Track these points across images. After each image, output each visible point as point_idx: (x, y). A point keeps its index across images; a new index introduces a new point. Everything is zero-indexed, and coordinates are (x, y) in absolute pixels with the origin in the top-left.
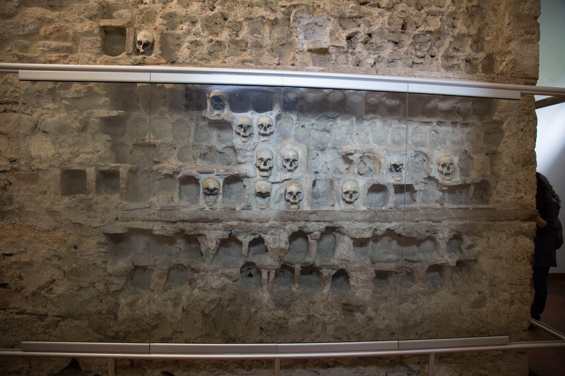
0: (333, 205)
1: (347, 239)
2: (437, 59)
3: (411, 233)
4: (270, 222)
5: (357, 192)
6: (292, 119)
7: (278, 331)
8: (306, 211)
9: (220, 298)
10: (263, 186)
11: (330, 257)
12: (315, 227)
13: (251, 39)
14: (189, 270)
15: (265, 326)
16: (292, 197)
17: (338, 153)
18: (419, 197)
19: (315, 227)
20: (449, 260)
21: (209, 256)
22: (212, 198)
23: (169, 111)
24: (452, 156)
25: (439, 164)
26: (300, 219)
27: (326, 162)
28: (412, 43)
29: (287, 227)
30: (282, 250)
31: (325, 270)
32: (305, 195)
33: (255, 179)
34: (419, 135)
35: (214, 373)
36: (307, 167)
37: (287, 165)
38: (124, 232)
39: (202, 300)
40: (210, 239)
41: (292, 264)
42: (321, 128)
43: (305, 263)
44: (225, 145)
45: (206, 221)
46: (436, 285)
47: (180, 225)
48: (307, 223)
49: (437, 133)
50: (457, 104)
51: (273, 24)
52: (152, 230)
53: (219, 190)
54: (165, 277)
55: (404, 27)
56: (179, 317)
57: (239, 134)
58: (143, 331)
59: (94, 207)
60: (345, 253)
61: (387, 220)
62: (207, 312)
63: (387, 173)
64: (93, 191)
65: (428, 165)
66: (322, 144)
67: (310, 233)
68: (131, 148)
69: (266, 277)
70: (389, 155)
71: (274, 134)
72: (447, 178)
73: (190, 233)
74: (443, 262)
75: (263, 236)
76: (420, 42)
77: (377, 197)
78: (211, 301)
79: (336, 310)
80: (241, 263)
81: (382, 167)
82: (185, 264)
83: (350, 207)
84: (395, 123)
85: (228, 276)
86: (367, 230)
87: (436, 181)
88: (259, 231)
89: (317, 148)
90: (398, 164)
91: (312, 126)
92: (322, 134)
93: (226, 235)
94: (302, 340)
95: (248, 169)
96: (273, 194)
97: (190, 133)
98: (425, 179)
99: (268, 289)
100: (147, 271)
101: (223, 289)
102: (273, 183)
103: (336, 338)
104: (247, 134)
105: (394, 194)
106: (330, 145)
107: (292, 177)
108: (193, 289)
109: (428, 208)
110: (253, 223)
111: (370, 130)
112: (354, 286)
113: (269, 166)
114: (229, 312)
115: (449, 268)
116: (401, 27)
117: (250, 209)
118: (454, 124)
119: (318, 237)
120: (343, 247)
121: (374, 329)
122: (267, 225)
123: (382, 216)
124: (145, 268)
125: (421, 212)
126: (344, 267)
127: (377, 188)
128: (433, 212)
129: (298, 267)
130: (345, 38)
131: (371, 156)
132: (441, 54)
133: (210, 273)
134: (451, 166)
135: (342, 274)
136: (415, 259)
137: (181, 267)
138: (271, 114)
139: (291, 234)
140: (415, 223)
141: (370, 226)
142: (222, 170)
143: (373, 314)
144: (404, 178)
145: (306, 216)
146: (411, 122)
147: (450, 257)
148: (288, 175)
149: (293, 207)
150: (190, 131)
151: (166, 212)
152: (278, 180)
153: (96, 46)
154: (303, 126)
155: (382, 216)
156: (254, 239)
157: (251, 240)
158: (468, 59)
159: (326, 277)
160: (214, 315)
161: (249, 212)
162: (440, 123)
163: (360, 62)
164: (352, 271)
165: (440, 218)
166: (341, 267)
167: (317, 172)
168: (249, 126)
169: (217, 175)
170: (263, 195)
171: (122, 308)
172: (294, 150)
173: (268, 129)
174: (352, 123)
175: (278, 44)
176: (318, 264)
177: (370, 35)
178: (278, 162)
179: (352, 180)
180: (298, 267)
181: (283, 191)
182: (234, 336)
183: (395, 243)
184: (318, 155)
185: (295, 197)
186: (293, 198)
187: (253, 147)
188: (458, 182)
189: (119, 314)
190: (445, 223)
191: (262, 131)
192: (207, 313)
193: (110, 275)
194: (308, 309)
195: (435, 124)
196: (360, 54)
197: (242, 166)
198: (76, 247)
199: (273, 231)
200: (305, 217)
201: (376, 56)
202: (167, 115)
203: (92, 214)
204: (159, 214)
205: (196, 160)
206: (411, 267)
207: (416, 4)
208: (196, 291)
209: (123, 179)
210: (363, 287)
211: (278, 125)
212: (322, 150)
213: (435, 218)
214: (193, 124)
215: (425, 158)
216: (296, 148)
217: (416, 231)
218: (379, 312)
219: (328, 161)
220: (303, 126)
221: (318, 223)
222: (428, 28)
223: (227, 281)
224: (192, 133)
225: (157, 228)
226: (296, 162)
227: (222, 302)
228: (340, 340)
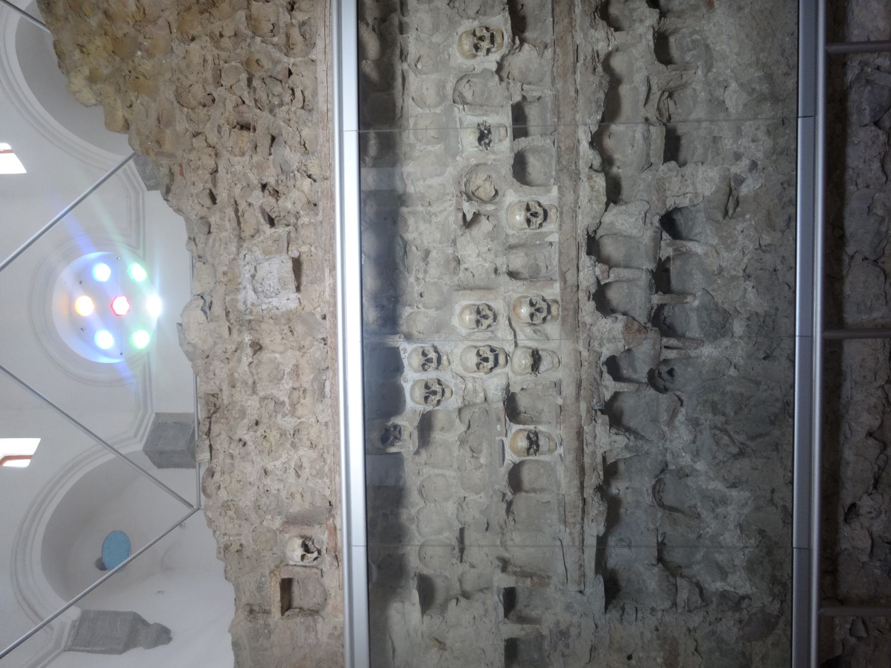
0: (551, 244)
1: (608, 218)
2: (293, 64)
3: (597, 102)
4: (581, 349)
5: (528, 205)
6: (411, 313)
7: (770, 332)
8: (561, 290)
9: (711, 429)
10: (522, 360)
11: (640, 242)
12: (589, 273)
13: (287, 384)
14: (662, 476)
15: (761, 352)
16: (538, 314)
17: (462, 235)
18: (533, 92)
19: (589, 273)
20: (648, 23)
21: (639, 445)
22: (542, 442)
23: (407, 508)
24: (461, 30)
25: (475, 56)
26: (575, 300)
27: (478, 255)
28: (271, 111)
29: (588, 320)
30: (627, 327)
31: (662, 252)
32: (533, 293)
33: (511, 375)
34: (425, 91)
35: (849, 436)
36: (487, 288)
37: (486, 323)
38: (602, 579)
39: (714, 458)
40: (610, 444)
41: (652, 308)
42: (422, 264)
43: (650, 288)
44: (457, 421)
45: (580, 451)
46: (693, 41)
47: (589, 492)
48: (580, 288)
49: (419, 58)
50: (368, 24)
51: (261, 348)
52: (598, 536)
53: (530, 431)
54: (676, 514)
55: (245, 127)
56: (747, 494)
57: (439, 402)
58: (769, 553)
59: (563, 627)
60: (633, 220)
61: (574, 149)
62: (734, 450)
63: (493, 153)
64: (538, 630)
65: (477, 74)
66: (447, 262)
67: (598, 281)
68: (466, 566)
69: (675, 351)
70: (462, 152)
71: (436, 344)
72: (498, 39)
73: (602, 477)
74: (650, 36)
75: (603, 359)
76: (268, 96)
77: (535, 166)
78: (717, 443)
79: (735, 229)
80: (651, 391)
81: (483, 161)
82: (653, 482)
83: (552, 214)
84: (408, 138)
85: (673, 415)
86: (593, 183)
87: (503, 58)
88: (596, 367)
89: (455, 271)
90: (477, 135)
91: (421, 281)
92: (432, 264)
93: (602, 419)
94: (790, 288)
95: (493, 385)
96: (534, 345)
97: (439, 475)
98: (501, 79)
99: (696, 348)
100: (665, 541)
101: (695, 423)
102: (516, 345)
103: (788, 226)
104: (437, 388)
105: (530, 138)
106: (450, 251)
107: (505, 315)
108: (696, 470)
109: (552, 72)
110: (584, 377)
111: (421, 182)
112: (691, 200)
113: (489, 353)
114: (736, 413)
115: (662, 22)
116: (245, 133)
117: (560, 381)
118: (402, 28)
119: (606, 267)
120: (623, 224)
121: (774, 157)
122: (585, 354)
123: (567, 157)
124: (661, 546)
125: (559, 86)
126: (658, 218)
127: (520, 168)
128: (560, 63)
129: (656, 299)
130: (273, 230)
131: (465, 180)
132: (285, 59)
133: (668, 445)
134: (478, 34)
135: (670, 223)
136: (643, 89)
137: (657, 487)
138: (405, 351)
139: (599, 314)
140: (580, 96)
141: (585, 179)
142: (498, 426)
143: (745, 163)
144: (502, 119)
145: (569, 290)
146: (405, 109)
147: (641, 21)
148: (503, 320)
149: (554, 309)
150: (437, 475)
151: (568, 515)
152: (510, 337)
153: (312, 624)
154: (421, 295)
155: (567, 157)
156: (609, 372)
157: (611, 378)
158: (289, 7)
159: (675, 250)
160: (740, 438)
161: (564, 384)
162: (403, 56)
163: (309, 202)
164: (665, 204)
165: (570, 48)
166: (658, 224)
167: (496, 270)
168: (427, 387)
169: (506, 436)
170: (536, 358)
171: (731, 586)
172: (462, 313)
173: (429, 356)
174: (414, 213)
175: (291, 339)
176: (652, 266)
177: (264, 187)
178: (482, 339)
179: (507, 213)
180: (656, 299)
181: (528, 330)
182: (779, 405)
183: (613, 127)
184: (466, 269)
185: (538, 310)
186: (540, 311)
187: (460, 379)
188: (506, 19)
189: (741, 592)
190: (579, 38)
191: (434, 365)
192: (737, 450)
193: (675, 604)
194: (734, 278)
195: (405, 66)
196: (297, 202)
197: (490, 396)
198: (630, 658)
199: (596, 344)
200: (572, 291)
201: (298, 175)
202: (413, 511)
203: (574, 631)
204: (572, 526)
205: (482, 465)
206: (659, 93)
207: (204, 106)
208: (700, 466)
209: (517, 582)
210: (693, 184)
211: (421, 335)
212: (459, 262)
213: (571, 59)
214: (425, 471)
215: (465, 80)
216: (458, 309)
217: (594, 93)
218: (742, 150)
219: (477, 251)
220: (421, 295)
221: (581, 269)
222: (244, 83)
223: (681, 417)
224: (440, 471)
225: (595, 528)
226: (481, 308)
227: (719, 425)
228: (792, 219)
